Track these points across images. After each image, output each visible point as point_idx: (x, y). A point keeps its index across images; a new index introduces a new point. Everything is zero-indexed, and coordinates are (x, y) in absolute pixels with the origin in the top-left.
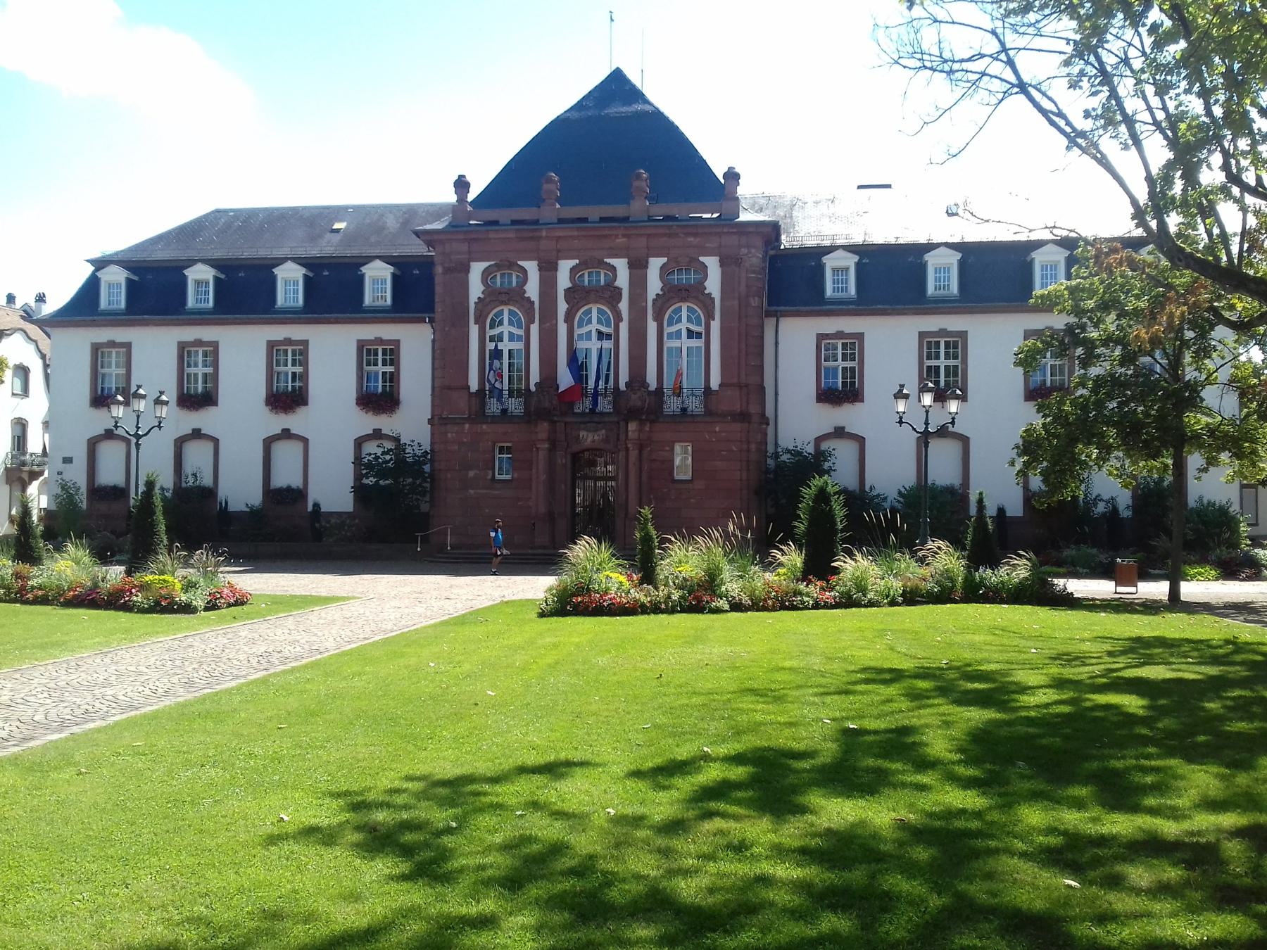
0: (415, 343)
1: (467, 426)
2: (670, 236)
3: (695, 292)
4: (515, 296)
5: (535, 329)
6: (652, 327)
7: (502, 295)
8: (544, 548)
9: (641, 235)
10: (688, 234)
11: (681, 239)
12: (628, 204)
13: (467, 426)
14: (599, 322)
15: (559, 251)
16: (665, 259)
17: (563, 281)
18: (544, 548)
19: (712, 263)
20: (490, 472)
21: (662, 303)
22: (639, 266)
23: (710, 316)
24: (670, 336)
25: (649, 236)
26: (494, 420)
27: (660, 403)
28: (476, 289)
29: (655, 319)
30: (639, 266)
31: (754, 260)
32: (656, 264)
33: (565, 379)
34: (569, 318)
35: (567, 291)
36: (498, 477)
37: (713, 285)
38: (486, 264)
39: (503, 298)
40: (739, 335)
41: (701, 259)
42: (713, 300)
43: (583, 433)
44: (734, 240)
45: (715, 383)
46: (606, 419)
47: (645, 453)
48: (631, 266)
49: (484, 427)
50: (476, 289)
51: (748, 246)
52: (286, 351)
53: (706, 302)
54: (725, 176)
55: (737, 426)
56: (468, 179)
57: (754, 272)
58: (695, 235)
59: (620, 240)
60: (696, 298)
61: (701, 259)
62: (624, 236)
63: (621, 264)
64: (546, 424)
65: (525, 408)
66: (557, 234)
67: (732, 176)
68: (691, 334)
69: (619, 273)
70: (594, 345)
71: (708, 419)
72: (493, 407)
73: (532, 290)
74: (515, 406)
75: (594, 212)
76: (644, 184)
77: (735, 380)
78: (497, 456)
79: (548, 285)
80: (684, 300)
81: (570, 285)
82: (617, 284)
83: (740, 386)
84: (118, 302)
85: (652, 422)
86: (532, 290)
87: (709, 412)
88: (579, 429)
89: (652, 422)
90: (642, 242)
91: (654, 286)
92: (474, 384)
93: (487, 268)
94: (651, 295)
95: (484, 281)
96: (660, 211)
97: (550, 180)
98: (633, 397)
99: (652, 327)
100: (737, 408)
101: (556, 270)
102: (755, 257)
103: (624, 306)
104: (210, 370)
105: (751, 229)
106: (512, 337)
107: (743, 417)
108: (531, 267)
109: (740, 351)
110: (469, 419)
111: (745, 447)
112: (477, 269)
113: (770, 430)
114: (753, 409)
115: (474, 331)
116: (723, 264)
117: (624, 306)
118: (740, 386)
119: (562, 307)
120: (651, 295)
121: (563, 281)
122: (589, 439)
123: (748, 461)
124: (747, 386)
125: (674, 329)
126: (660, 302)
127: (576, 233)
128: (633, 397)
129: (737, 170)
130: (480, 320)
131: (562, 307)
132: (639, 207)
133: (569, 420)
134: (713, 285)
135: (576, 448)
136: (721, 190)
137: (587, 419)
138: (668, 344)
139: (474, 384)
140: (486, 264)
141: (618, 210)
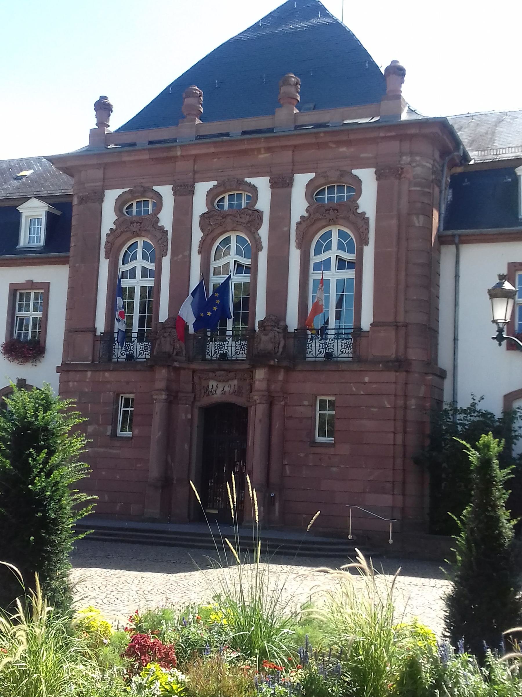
0: (57, 278)
1: (89, 374)
2: (319, 146)
3: (344, 211)
4: (147, 224)
5: (166, 261)
6: (295, 256)
7: (136, 223)
8: (153, 520)
9: (285, 148)
10: (339, 143)
11: (325, 147)
12: (273, 113)
13: (89, 374)
14: (340, 247)
15: (195, 172)
16: (312, 175)
17: (200, 205)
18: (153, 520)
19: (367, 177)
20: (110, 428)
21: (308, 228)
22: (282, 184)
23: (363, 240)
24: (317, 266)
25: (295, 148)
26: (119, 367)
27: (303, 349)
28: (109, 219)
29: (299, 246)
30: (282, 184)
31: (419, 170)
32: (302, 181)
33: (292, 321)
34: (205, 249)
35: (203, 217)
36: (120, 433)
37: (368, 203)
38: (120, 191)
39: (135, 228)
40: (398, 260)
41: (355, 172)
42: (366, 221)
43: (212, 383)
44: (394, 146)
45: (367, 320)
46: (237, 367)
47: (277, 407)
48: (273, 185)
49: (107, 374)
50: (109, 219)
51: (411, 153)
52: (29, 294)
53: (360, 223)
54: (387, 70)
55: (391, 376)
56: (111, 101)
57: (417, 184)
58: (348, 143)
59: (264, 156)
60: (346, 218)
61: (355, 172)
62: (268, 150)
63: (262, 184)
64: (164, 371)
65: (354, 352)
66: (194, 152)
67: (397, 71)
68: (342, 264)
69: (260, 194)
70: (334, 275)
71: (355, 367)
72: (119, 353)
73: (166, 219)
74: (140, 351)
75: (235, 127)
76: (292, 90)
77: (391, 319)
78: (122, 409)
79: (183, 212)
80: (333, 222)
81: (206, 210)
82: (258, 206)
83: (396, 326)
84: (38, 238)
85: (288, 370)
86: (166, 219)
87: (358, 359)
88: (209, 379)
89: (288, 370)
90: (287, 156)
91: (299, 206)
92: (101, 326)
93: (120, 196)
94: (295, 218)
95: (309, 195)
96: (309, 118)
97: (192, 95)
98: (264, 338)
99: (295, 256)
100: (391, 353)
101: (103, 201)
102: (421, 164)
103: (264, 232)
104: (39, 314)
105: (413, 131)
106: (145, 273)
107: (400, 364)
108: (166, 191)
109: (397, 283)
110: (94, 366)
111: (400, 402)
112: (112, 196)
113: (447, 384)
114: (415, 354)
115: (104, 265)
116: (379, 176)
117: (264, 232)
118: (396, 326)
119: (197, 235)
120: (295, 218)
121: (200, 205)
122: (219, 391)
123: (405, 421)
124: (406, 325)
125: (324, 257)
126: (304, 225)
127: (212, 150)
128: (264, 338)
129: (401, 64)
130: (112, 253)
131: (197, 235)
132: (288, 114)
133: (195, 366)
134: (368, 203)
135: (205, 401)
136: (380, 84)
137: (216, 366)
138: (315, 276)
139: (101, 326)
140: (120, 191)
141: (262, 122)
